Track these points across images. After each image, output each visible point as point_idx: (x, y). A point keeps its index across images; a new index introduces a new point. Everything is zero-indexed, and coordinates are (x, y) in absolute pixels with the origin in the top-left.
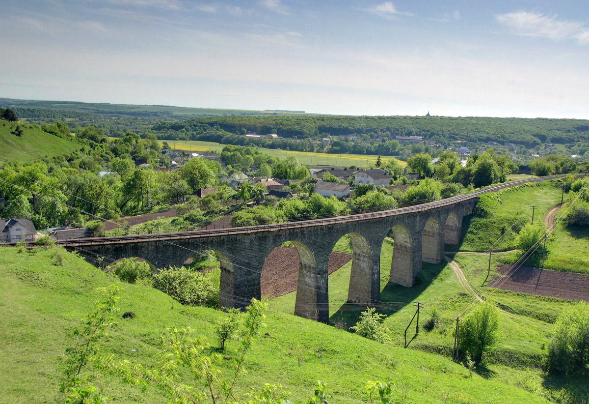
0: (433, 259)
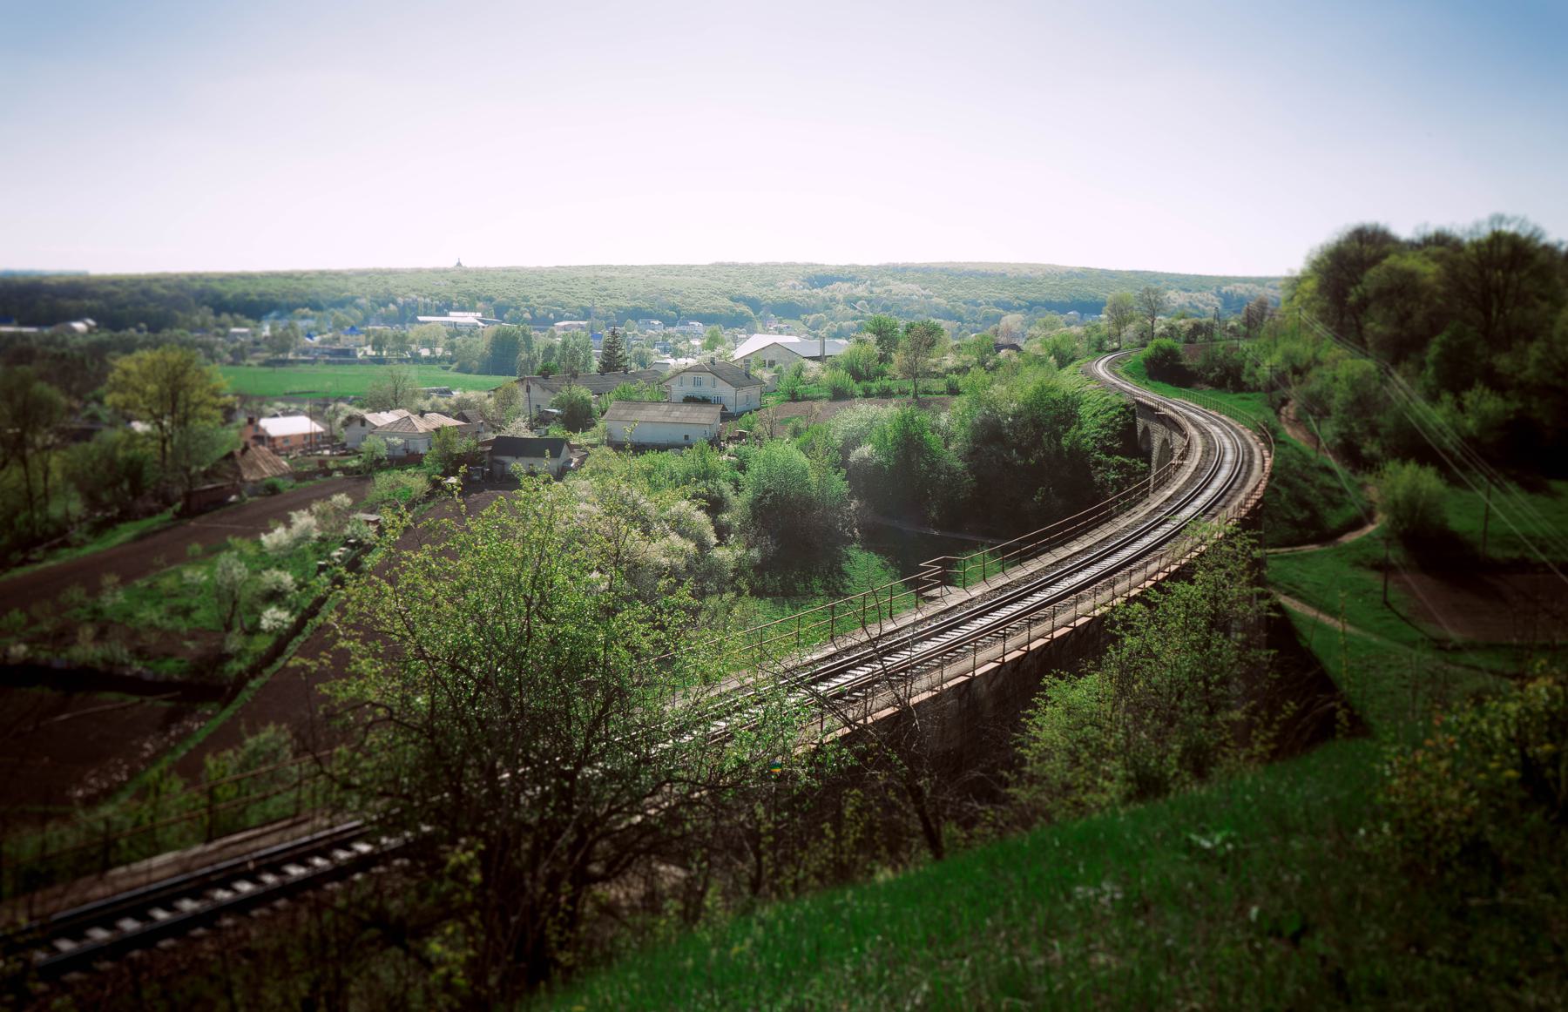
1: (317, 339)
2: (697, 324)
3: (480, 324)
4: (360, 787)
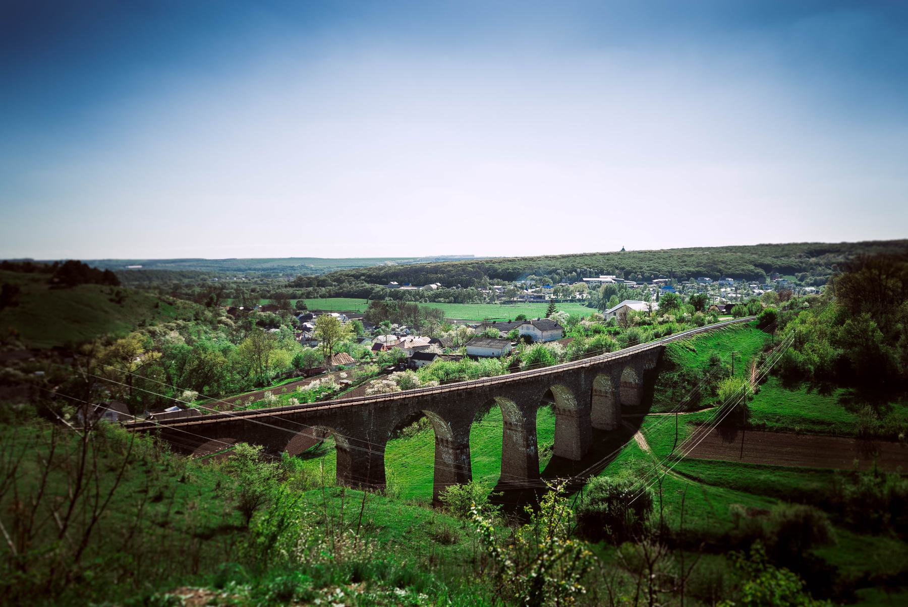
0: (608, 424)
1: (530, 291)
2: (730, 279)
3: (613, 281)
4: (285, 470)
